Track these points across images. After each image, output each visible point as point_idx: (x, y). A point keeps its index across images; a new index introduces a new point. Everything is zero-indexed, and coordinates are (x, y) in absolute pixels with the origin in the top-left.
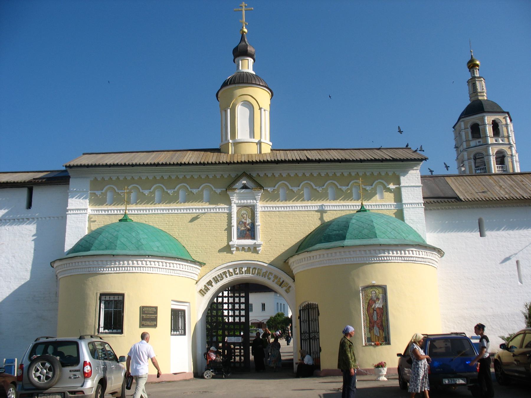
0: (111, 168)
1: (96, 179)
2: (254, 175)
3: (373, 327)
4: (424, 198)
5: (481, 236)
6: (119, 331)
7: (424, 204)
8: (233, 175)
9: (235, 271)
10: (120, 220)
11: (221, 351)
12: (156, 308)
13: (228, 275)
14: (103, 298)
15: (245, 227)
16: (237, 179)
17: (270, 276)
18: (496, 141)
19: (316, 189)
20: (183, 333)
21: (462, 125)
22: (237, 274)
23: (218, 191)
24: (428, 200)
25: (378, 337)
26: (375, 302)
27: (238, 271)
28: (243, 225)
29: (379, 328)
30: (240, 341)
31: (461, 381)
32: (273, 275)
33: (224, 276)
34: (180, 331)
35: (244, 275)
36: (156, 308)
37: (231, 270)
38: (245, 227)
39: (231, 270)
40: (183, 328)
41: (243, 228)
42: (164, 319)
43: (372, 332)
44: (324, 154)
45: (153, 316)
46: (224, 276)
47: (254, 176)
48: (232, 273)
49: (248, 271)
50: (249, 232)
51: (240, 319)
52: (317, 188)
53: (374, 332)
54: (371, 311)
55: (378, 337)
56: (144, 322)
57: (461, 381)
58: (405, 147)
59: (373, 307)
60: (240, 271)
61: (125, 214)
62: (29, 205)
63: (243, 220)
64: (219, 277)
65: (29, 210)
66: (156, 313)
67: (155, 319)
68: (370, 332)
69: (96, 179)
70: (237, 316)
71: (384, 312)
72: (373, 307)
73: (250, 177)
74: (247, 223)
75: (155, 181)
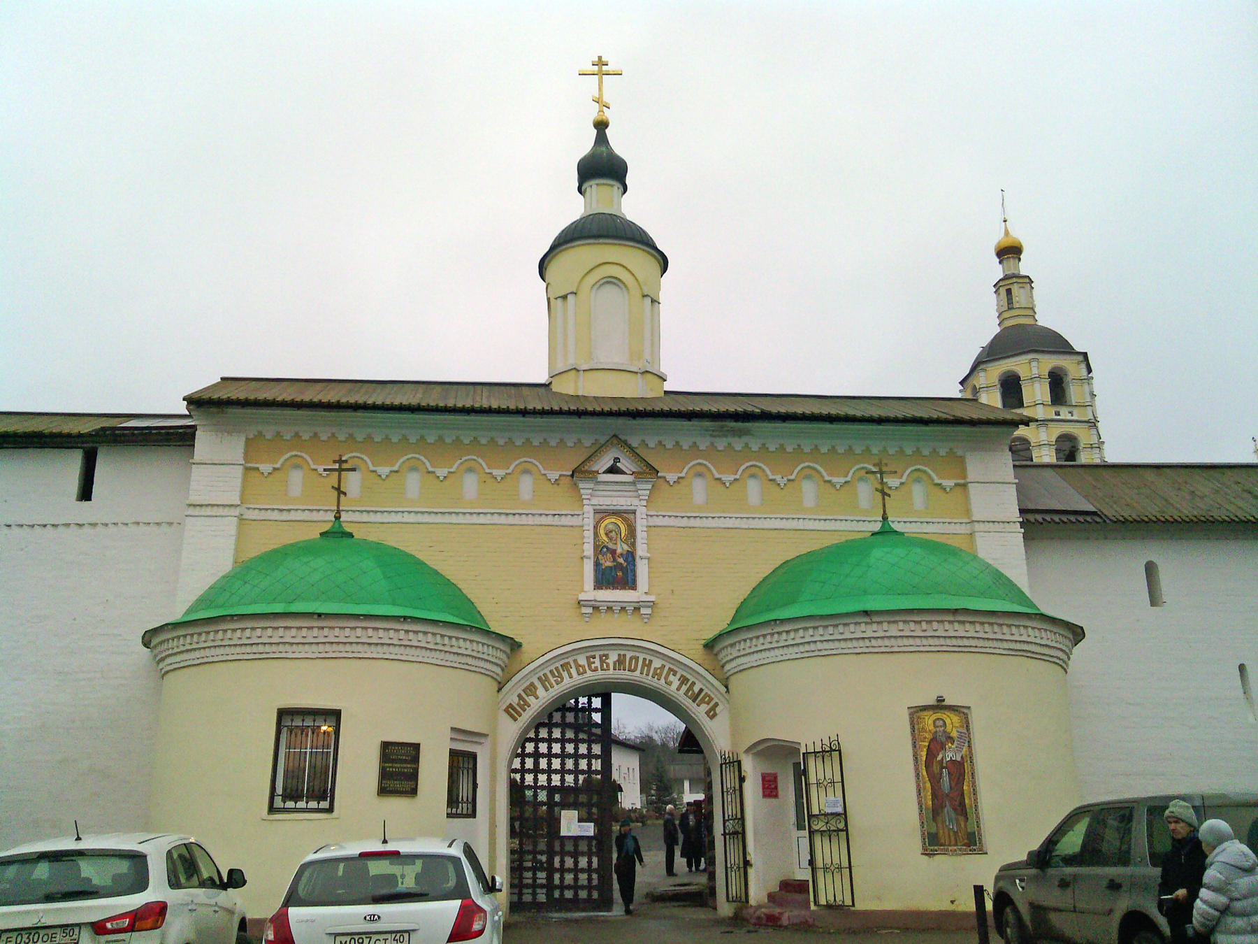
0: (300, 412)
3: (943, 807)
5: (1152, 605)
6: (324, 804)
7: (1022, 524)
9: (589, 664)
11: (544, 858)
12: (416, 747)
13: (573, 671)
14: (287, 722)
15: (614, 560)
17: (671, 678)
18: (1058, 414)
20: (470, 811)
21: (981, 379)
22: (596, 670)
25: (956, 833)
26: (943, 747)
27: (597, 663)
28: (609, 555)
29: (955, 809)
30: (592, 834)
32: (678, 676)
33: (565, 674)
35: (600, 672)
36: (416, 747)
37: (582, 661)
38: (614, 560)
39: (582, 661)
41: (609, 564)
42: (433, 772)
43: (939, 819)
46: (565, 674)
47: (634, 445)
48: (583, 667)
49: (620, 662)
50: (616, 572)
51: (563, 780)
53: (944, 822)
54: (936, 769)
55: (956, 833)
56: (387, 783)
59: (939, 758)
60: (602, 662)
62: (86, 493)
63: (611, 546)
64: (554, 676)
65: (85, 504)
66: (416, 759)
67: (414, 776)
68: (934, 819)
70: (556, 772)
71: (960, 771)
72: (939, 758)
74: (619, 551)
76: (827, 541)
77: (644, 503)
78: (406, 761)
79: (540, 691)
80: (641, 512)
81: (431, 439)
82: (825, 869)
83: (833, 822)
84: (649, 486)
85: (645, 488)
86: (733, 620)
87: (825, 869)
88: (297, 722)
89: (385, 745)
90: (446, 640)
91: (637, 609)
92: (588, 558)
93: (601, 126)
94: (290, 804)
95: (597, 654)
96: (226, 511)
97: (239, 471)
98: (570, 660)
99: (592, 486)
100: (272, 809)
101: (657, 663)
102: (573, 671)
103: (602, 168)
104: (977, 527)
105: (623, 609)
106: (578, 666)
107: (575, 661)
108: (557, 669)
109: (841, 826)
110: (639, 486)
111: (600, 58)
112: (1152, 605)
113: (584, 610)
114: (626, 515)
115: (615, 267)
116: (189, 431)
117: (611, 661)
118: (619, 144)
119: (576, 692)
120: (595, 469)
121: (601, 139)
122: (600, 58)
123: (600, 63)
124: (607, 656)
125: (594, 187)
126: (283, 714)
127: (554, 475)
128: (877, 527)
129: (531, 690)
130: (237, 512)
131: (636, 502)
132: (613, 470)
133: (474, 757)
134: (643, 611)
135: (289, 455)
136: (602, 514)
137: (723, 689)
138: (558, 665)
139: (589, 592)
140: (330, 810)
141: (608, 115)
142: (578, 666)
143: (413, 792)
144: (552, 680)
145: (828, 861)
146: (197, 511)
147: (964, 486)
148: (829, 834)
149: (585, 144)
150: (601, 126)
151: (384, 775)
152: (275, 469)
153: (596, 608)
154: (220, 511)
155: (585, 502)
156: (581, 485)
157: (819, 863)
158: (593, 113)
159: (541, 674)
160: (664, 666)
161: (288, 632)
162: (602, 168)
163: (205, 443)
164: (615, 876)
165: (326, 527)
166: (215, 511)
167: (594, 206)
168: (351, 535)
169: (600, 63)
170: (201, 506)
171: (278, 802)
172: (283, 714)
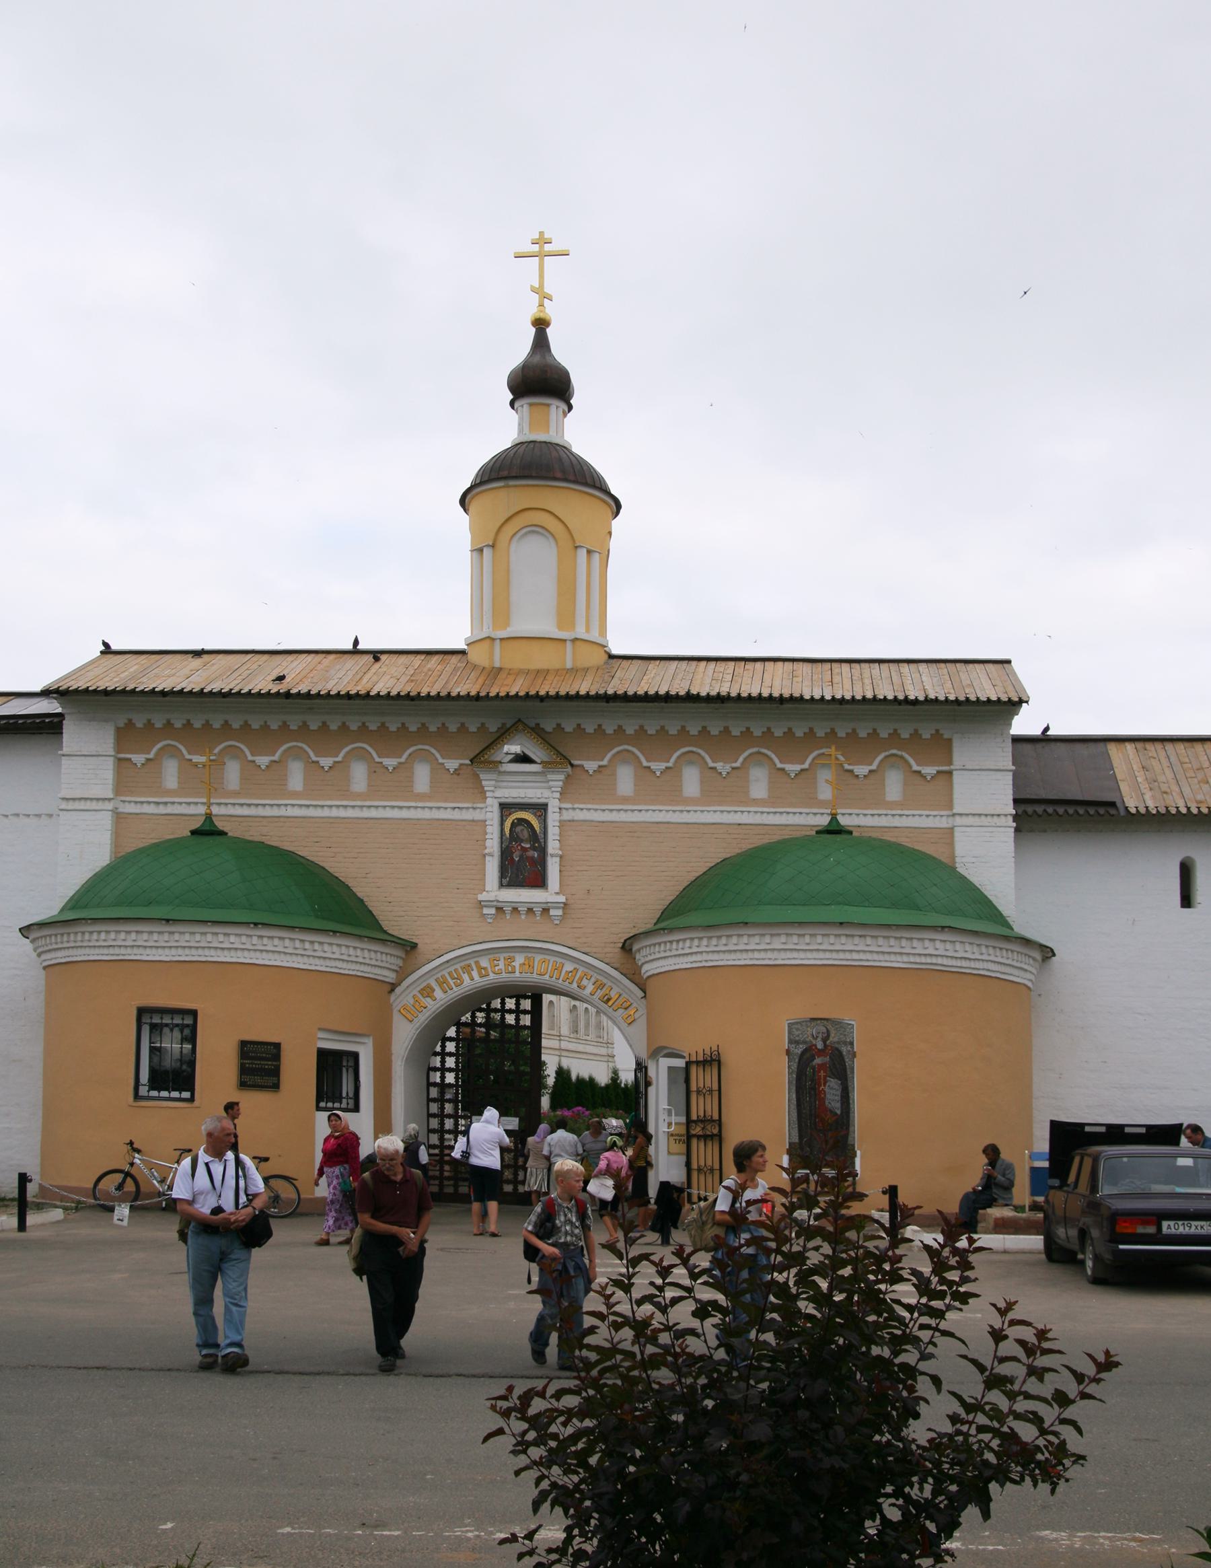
1: (130, 724)
2: (549, 726)
4: (1016, 801)
5: (1183, 906)
6: (186, 1095)
7: (1016, 818)
8: (493, 727)
10: (193, 832)
12: (277, 1046)
16: (503, 735)
19: (714, 768)
20: (351, 1106)
23: (452, 764)
24: (1022, 808)
31: (169, 1525)
33: (466, 977)
34: (344, 1101)
36: (277, 1046)
39: (484, 962)
40: (351, 1095)
42: (299, 1072)
44: (987, 685)
45: (269, 1064)
47: (549, 729)
48: (485, 969)
52: (719, 766)
57: (169, 1525)
58: (350, 647)
61: (209, 817)
67: (276, 1072)
69: (130, 724)
73: (538, 733)
75: (683, 737)
76: (786, 834)
77: (558, 795)
78: (268, 1059)
79: (438, 993)
80: (553, 806)
81: (314, 726)
82: (699, 1170)
83: (709, 1127)
84: (562, 777)
85: (557, 779)
86: (659, 921)
87: (699, 1170)
88: (156, 1020)
89: (243, 1044)
90: (307, 945)
91: (546, 911)
92: (491, 855)
93: (541, 325)
94: (154, 1093)
95: (502, 956)
96: (100, 805)
97: (109, 764)
98: (472, 962)
99: (494, 776)
100: (137, 1096)
101: (569, 967)
102: (475, 974)
103: (541, 382)
104: (959, 821)
105: (530, 910)
106: (480, 968)
107: (477, 963)
108: (456, 970)
109: (716, 1131)
110: (550, 777)
111: (541, 233)
112: (1183, 906)
113: (486, 911)
114: (541, 809)
115: (547, 515)
116: (56, 720)
117: (517, 964)
118: (562, 352)
119: (504, 991)
120: (498, 759)
121: (541, 342)
122: (541, 233)
123: (542, 240)
124: (512, 959)
125: (526, 408)
126: (142, 1012)
127: (452, 764)
128: (824, 821)
129: (428, 992)
130: (110, 806)
131: (547, 793)
132: (523, 759)
133: (355, 1056)
134: (552, 912)
135: (159, 746)
136: (506, 808)
137: (641, 994)
138: (458, 966)
139: (492, 889)
140: (192, 1099)
141: (551, 311)
142: (480, 968)
143: (276, 1087)
144: (452, 982)
145: (702, 1163)
146: (71, 805)
147: (950, 773)
148: (705, 1138)
149: (519, 351)
150: (541, 325)
151: (243, 1070)
152: (148, 760)
153: (499, 909)
154: (94, 805)
155: (488, 794)
156: (482, 776)
157: (694, 1166)
158: (531, 310)
159: (439, 975)
160: (576, 970)
161: (140, 936)
162: (541, 382)
163: (74, 736)
164: (1121, 1247)
165: (196, 825)
166: (89, 805)
167: (526, 430)
168: (222, 833)
169: (542, 240)
170: (74, 799)
171: (143, 1091)
172: (142, 1012)
